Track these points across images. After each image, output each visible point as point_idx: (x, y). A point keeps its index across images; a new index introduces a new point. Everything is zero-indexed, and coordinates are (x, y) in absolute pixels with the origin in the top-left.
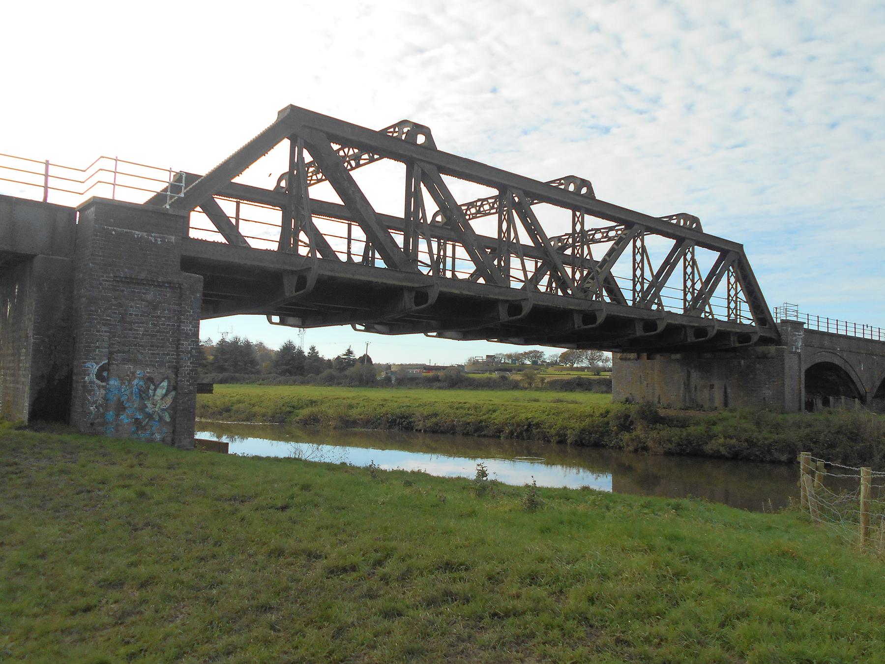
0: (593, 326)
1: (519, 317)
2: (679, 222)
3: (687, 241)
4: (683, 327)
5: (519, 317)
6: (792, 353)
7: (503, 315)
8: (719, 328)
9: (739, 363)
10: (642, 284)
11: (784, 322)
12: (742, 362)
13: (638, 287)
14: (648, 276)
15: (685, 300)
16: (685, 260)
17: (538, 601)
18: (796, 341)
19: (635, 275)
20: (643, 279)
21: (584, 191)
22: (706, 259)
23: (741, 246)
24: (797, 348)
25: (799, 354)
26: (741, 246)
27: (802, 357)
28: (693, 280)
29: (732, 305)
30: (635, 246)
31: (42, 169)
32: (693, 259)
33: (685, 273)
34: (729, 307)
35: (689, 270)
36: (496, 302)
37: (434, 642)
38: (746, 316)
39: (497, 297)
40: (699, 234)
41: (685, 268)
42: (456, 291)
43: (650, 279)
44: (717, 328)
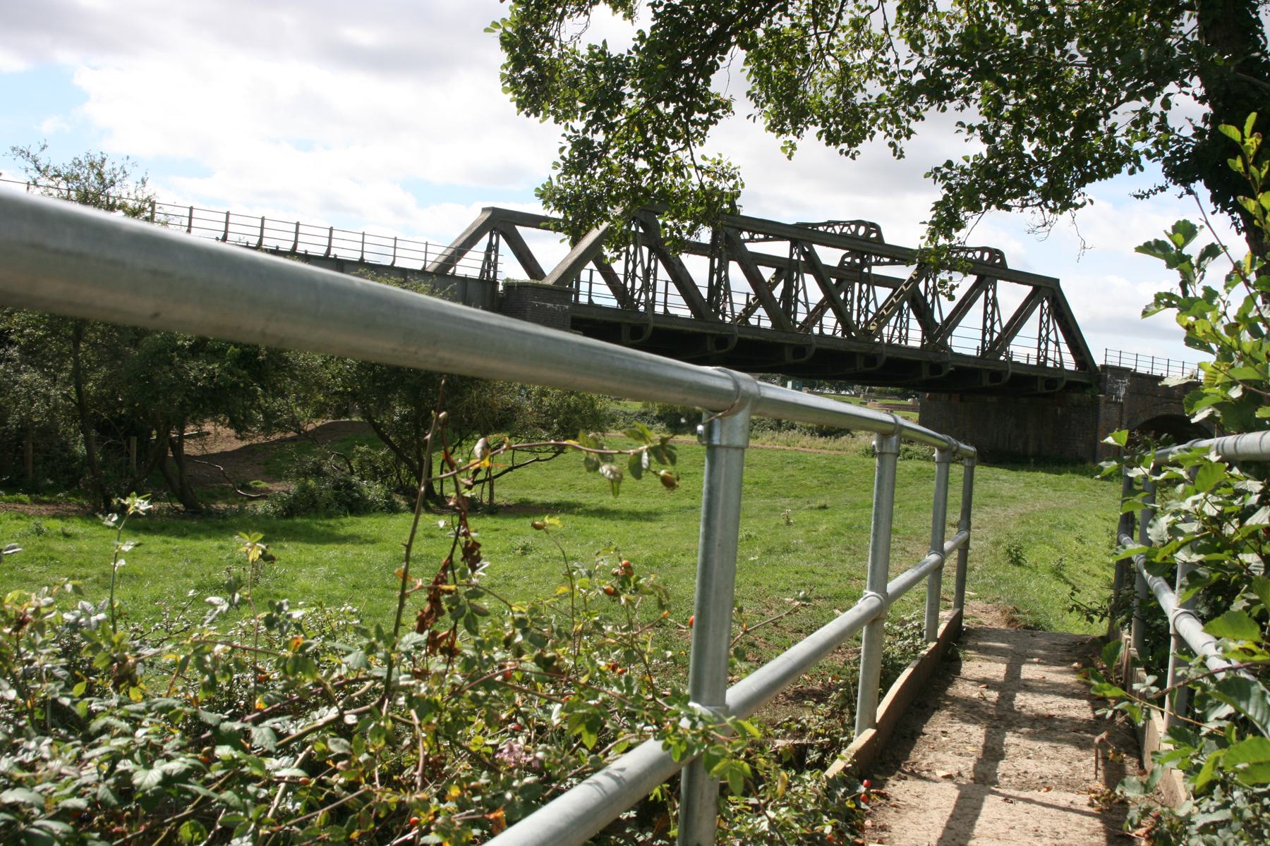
0: (873, 369)
1: (803, 360)
2: (982, 256)
3: (987, 279)
4: (919, 363)
5: (803, 360)
6: (1112, 402)
7: (926, 375)
8: (657, 325)
9: (1056, 411)
10: (866, 316)
11: (1105, 367)
12: (1059, 411)
13: (988, 337)
14: (997, 328)
15: (983, 340)
16: (1042, 307)
17: (45, 648)
18: (1118, 389)
19: (1040, 335)
20: (1048, 339)
21: (873, 235)
22: (1010, 296)
23: (1057, 281)
24: (1118, 397)
25: (1121, 404)
26: (1057, 281)
27: (1125, 408)
28: (867, 300)
29: (1043, 346)
30: (986, 297)
31: (392, 243)
32: (994, 297)
33: (1041, 321)
34: (1039, 349)
35: (989, 309)
36: (854, 354)
37: (909, 636)
38: (1070, 364)
39: (703, 331)
40: (1003, 271)
41: (1042, 316)
42: (749, 337)
43: (874, 311)
44: (652, 325)
